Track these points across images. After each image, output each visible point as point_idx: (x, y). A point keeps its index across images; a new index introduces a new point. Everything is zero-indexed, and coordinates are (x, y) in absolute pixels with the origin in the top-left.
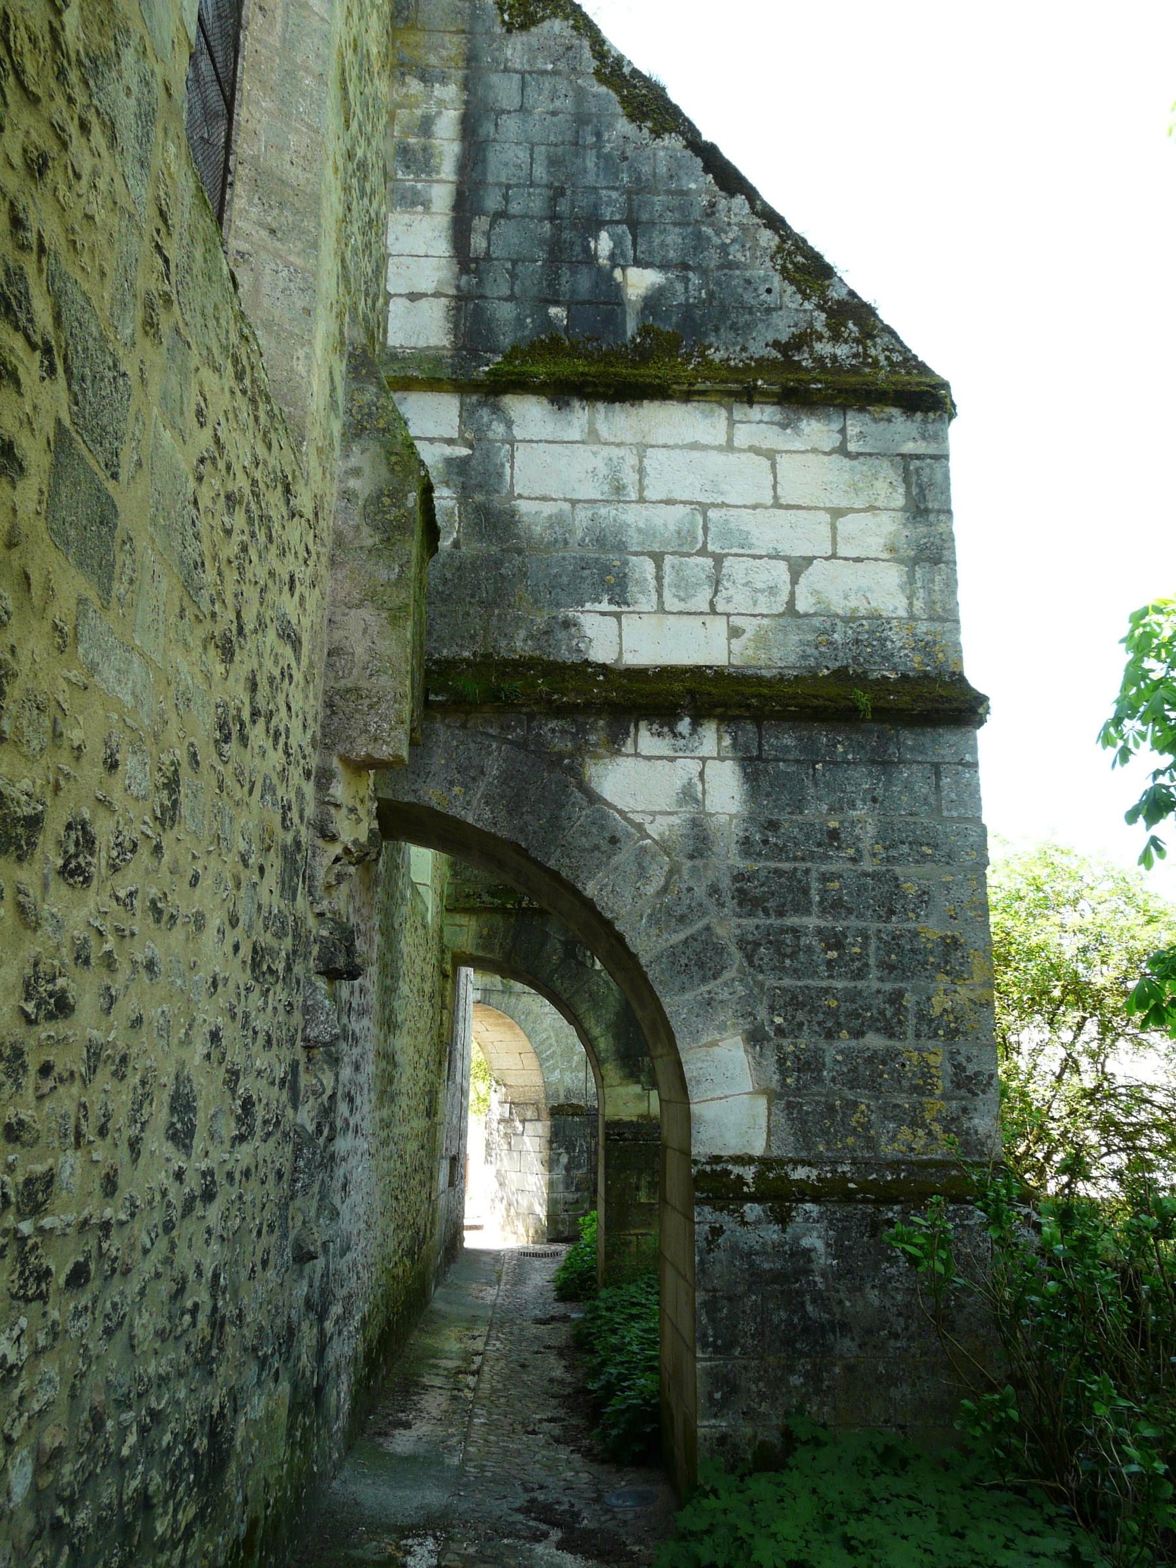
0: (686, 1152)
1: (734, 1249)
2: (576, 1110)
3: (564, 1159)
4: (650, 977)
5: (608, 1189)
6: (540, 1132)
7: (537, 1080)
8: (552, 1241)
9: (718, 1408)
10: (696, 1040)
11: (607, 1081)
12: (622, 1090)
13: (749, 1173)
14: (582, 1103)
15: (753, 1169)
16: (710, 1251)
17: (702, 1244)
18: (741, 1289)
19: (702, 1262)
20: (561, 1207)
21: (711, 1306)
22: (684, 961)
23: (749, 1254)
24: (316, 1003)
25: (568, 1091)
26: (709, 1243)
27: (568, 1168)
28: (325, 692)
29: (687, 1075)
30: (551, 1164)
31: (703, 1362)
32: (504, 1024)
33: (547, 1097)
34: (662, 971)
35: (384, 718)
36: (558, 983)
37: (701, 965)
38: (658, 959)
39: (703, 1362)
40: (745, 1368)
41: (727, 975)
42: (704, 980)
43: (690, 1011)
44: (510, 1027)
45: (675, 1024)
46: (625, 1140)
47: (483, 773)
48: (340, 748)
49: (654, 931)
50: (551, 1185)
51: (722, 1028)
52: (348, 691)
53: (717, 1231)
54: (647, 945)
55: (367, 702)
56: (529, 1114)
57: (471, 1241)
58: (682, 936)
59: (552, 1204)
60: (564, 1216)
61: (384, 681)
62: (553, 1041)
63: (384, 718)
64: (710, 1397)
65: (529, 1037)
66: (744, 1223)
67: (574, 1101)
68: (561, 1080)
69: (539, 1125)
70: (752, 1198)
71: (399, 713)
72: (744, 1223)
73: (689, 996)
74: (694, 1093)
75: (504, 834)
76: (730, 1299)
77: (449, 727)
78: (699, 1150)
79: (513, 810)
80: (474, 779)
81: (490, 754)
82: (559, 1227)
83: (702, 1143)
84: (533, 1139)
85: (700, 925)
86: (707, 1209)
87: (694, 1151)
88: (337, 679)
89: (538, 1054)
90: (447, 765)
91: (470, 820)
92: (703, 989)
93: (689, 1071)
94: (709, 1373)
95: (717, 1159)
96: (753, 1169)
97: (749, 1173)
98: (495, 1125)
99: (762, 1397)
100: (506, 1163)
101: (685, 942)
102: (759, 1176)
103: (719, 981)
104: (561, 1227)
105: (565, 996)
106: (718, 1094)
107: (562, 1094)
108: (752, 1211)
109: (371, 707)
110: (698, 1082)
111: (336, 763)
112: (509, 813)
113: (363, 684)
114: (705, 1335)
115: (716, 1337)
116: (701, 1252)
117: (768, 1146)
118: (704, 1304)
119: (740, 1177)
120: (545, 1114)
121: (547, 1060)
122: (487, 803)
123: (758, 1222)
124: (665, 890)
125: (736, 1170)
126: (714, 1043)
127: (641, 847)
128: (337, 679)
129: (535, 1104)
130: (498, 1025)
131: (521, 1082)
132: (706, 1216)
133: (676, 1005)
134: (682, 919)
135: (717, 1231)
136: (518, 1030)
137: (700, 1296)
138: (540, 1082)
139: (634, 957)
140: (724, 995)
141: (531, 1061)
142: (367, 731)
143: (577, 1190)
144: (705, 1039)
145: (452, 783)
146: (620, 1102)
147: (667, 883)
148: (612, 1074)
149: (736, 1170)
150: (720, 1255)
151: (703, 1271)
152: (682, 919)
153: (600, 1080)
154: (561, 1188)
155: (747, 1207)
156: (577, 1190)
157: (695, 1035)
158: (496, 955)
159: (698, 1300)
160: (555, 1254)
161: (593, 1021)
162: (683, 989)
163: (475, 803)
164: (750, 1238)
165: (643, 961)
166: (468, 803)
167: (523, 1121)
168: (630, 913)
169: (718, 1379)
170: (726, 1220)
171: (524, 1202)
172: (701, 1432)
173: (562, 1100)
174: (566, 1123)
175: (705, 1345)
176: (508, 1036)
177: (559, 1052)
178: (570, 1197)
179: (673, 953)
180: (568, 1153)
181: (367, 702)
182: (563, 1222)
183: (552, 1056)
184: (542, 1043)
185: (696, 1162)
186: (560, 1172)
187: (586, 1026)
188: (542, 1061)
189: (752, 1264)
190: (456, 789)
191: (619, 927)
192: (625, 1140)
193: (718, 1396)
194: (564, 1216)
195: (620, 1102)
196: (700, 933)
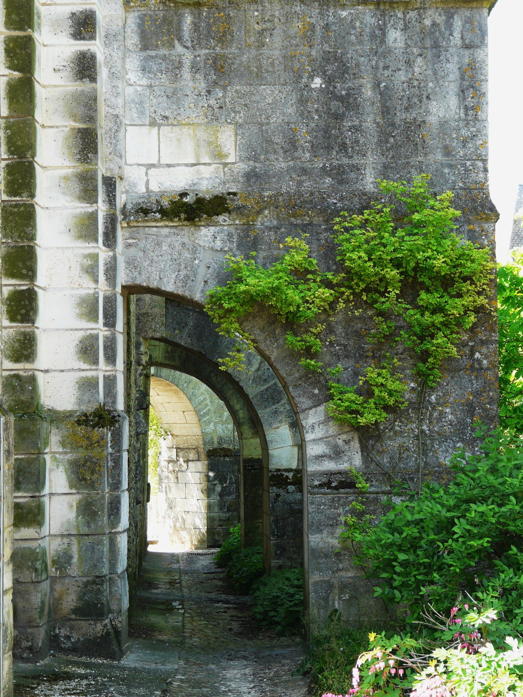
0: (268, 468)
1: (284, 502)
2: (227, 452)
3: (219, 488)
4: (253, 403)
5: (246, 497)
6: (200, 469)
7: (197, 431)
8: (209, 547)
9: (278, 556)
10: (271, 427)
11: (244, 436)
12: (253, 441)
13: (290, 475)
14: (231, 447)
15: (292, 473)
16: (276, 502)
17: (273, 500)
18: (287, 516)
19: (273, 506)
20: (217, 523)
21: (276, 522)
22: (266, 397)
23: (290, 504)
24: (140, 421)
25: (220, 438)
26: (275, 500)
27: (221, 495)
28: (136, 315)
29: (268, 440)
30: (209, 492)
31: (273, 541)
32: (171, 390)
33: (205, 444)
34: (258, 401)
35: (157, 323)
36: (214, 379)
37: (273, 398)
38: (256, 396)
39: (273, 541)
40: (288, 543)
41: (283, 402)
42: (274, 404)
43: (269, 415)
44: (176, 393)
45: (263, 421)
46: (255, 469)
47: (187, 325)
48: (143, 335)
49: (254, 385)
50: (209, 507)
51: (281, 422)
52: (144, 314)
53: (278, 496)
54: (252, 391)
55: (151, 318)
56: (192, 455)
57: (151, 549)
58: (265, 387)
59: (210, 520)
60: (219, 529)
61: (156, 310)
62: (208, 402)
63: (157, 323)
64: (276, 553)
65: (190, 399)
66: (288, 493)
67: (225, 446)
68: (215, 431)
69: (199, 464)
70: (291, 484)
71: (162, 321)
72: (288, 493)
73: (268, 410)
74: (270, 446)
75: (196, 349)
76: (283, 519)
77: (173, 306)
78: (272, 467)
79: (199, 339)
80: (183, 327)
81: (189, 317)
82: (213, 536)
83: (273, 464)
84: (195, 474)
85: (272, 383)
86: (274, 488)
87: (270, 467)
88: (140, 310)
89: (197, 412)
90: (173, 322)
91: (182, 344)
92: (274, 407)
93: (268, 438)
94: (275, 545)
95: (279, 470)
96: (292, 473)
97: (290, 475)
98: (164, 464)
99: (294, 552)
100: (175, 493)
101: (267, 389)
102: (294, 476)
103: (280, 404)
104: (216, 537)
105: (219, 386)
106: (279, 446)
107: (216, 440)
108: (291, 488)
109: (152, 319)
110: (272, 442)
111: (141, 339)
112: (198, 340)
113: (150, 311)
114: (274, 532)
115: (278, 532)
116: (272, 503)
117: (298, 465)
118: (273, 521)
119: (287, 476)
120: (203, 456)
121: (204, 416)
122: (189, 337)
123: (293, 492)
124: (258, 369)
125: (286, 474)
126: (278, 428)
127: (249, 353)
128: (140, 310)
129: (196, 449)
130: (167, 391)
131: (184, 432)
132: (274, 490)
133: (263, 413)
134: (265, 381)
135: (278, 496)
136: (182, 394)
137: (272, 518)
138: (199, 433)
139: (247, 396)
140: (282, 409)
141: (192, 417)
142: (151, 328)
143: (229, 511)
144: (274, 426)
145: (175, 329)
146: (252, 448)
147: (259, 366)
148: (247, 431)
149: (286, 474)
150: (279, 504)
151: (273, 510)
152: (265, 381)
153: (240, 435)
154: (216, 509)
155: (289, 487)
156: (229, 511)
157: (270, 425)
158: (177, 363)
159: (271, 520)
160: (212, 554)
161: (235, 401)
162: (266, 407)
163: (184, 337)
164: (290, 498)
165: (250, 397)
166: (182, 337)
167: (187, 461)
168: (245, 379)
169: (278, 546)
170: (282, 492)
171: (189, 518)
172: (272, 564)
173: (216, 445)
174: (219, 460)
175: (274, 535)
176: (174, 399)
177: (213, 409)
178: (224, 516)
179: (262, 394)
180: (221, 484)
181: (151, 318)
182: (218, 533)
183: (207, 414)
184: (200, 404)
185: (271, 471)
186: (215, 499)
187: (231, 403)
188: (200, 417)
189: (291, 507)
190: (177, 332)
191: (241, 384)
192: (255, 469)
193: (278, 552)
194: (219, 529)
195: (252, 448)
196: (272, 386)
